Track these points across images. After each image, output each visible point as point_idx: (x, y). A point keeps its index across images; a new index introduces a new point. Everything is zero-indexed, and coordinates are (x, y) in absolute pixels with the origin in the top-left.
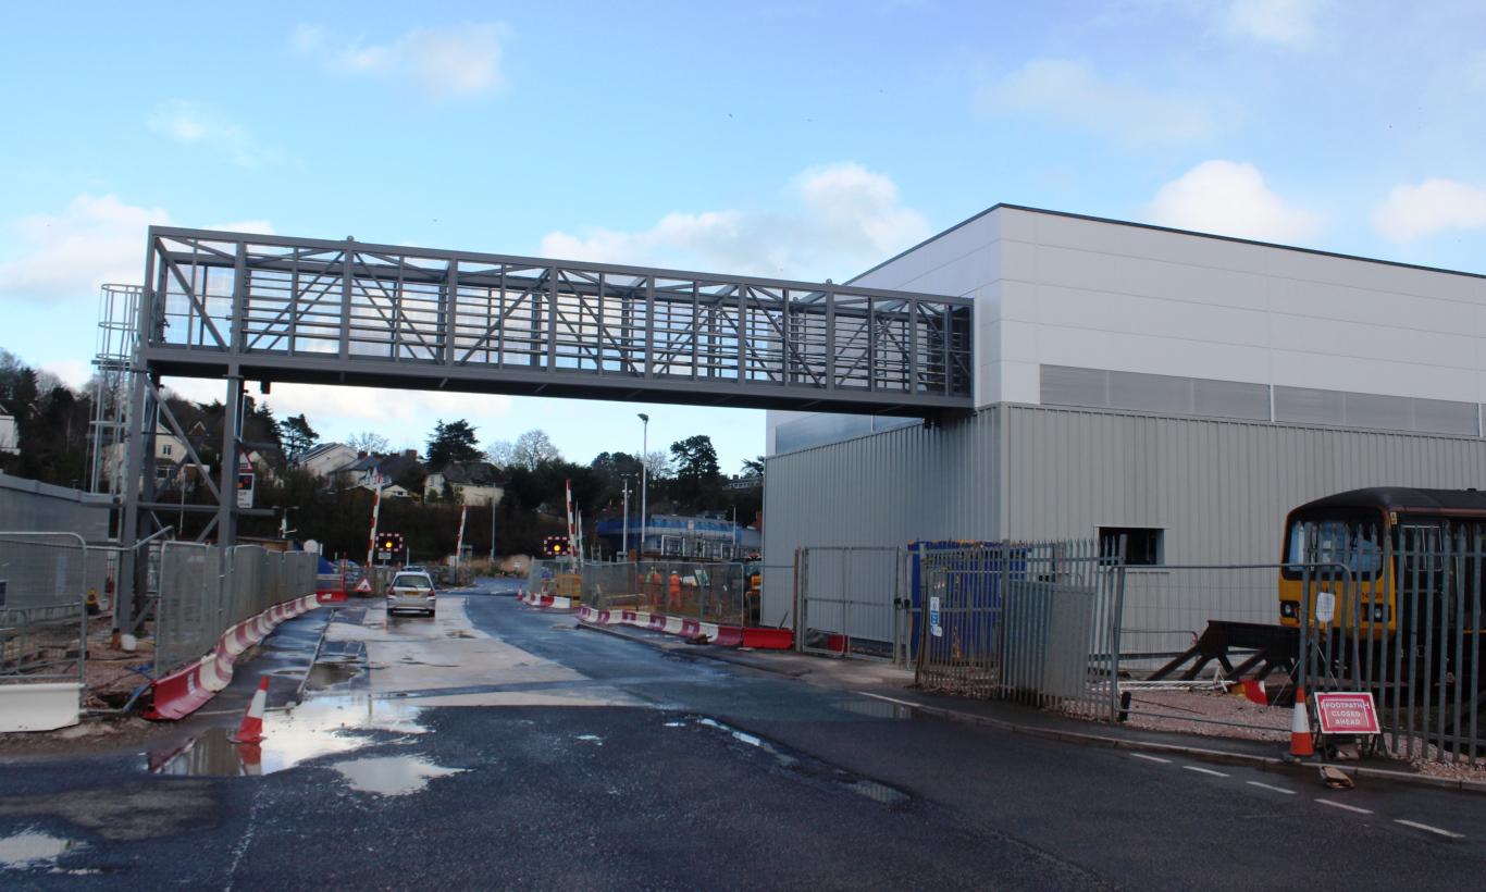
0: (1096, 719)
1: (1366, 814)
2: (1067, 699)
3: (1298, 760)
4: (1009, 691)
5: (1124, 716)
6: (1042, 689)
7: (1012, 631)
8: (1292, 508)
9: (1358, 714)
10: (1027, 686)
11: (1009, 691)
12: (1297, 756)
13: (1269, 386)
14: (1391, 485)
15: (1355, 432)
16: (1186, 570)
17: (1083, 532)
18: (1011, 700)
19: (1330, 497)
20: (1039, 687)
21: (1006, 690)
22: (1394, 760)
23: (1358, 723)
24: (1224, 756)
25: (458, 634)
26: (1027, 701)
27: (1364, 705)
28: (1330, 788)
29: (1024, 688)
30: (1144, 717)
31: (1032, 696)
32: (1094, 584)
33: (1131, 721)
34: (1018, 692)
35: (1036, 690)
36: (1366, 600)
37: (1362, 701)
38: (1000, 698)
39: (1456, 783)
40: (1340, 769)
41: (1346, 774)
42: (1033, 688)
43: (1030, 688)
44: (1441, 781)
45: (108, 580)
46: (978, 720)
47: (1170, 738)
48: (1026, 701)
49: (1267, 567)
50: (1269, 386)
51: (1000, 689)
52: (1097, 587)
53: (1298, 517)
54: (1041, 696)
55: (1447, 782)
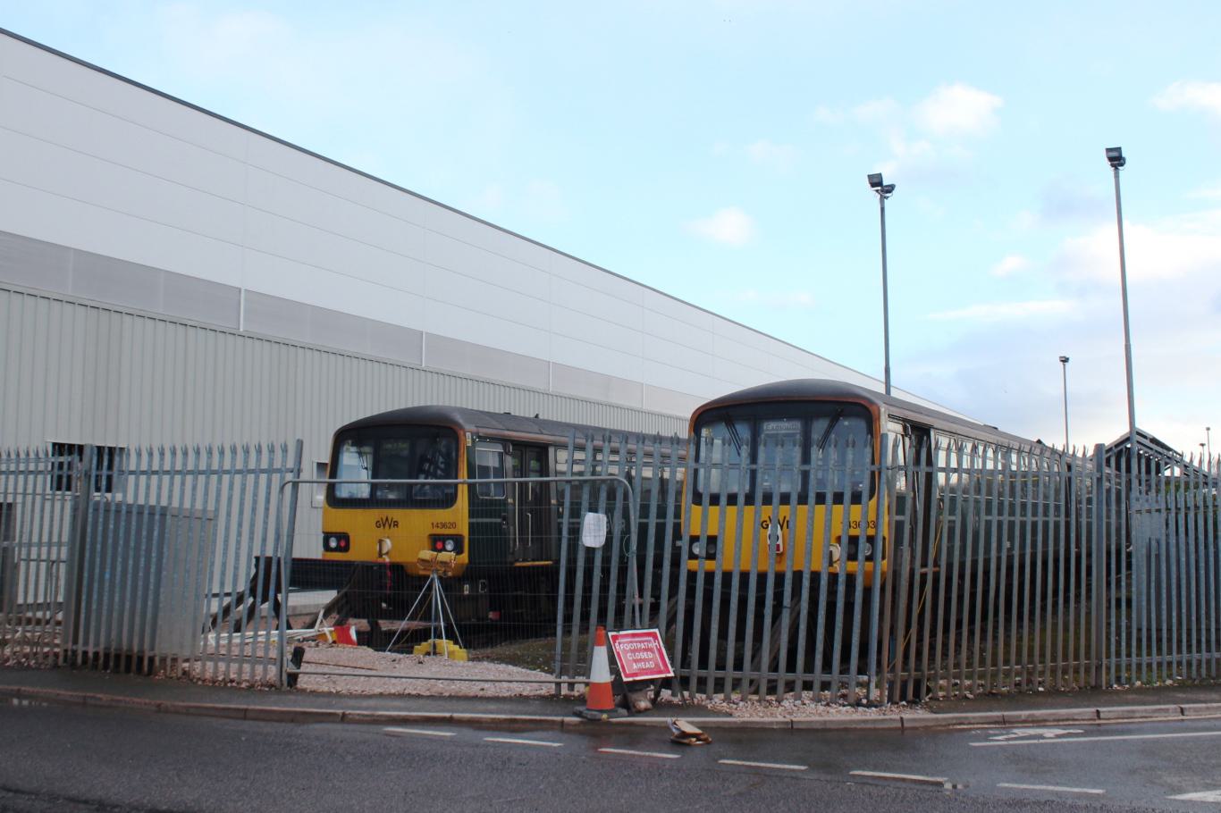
0: (251, 687)
1: (1003, 781)
2: (187, 660)
3: (605, 716)
4: (91, 655)
5: (293, 678)
6: (152, 648)
7: (97, 571)
8: (339, 426)
9: (650, 655)
10: (125, 647)
11: (91, 655)
12: (602, 711)
13: (240, 290)
14: (458, 405)
15: (317, 350)
16: (308, 484)
17: (1035, 440)
18: (95, 667)
19: (383, 414)
20: (146, 646)
21: (85, 653)
22: (678, 705)
23: (651, 665)
24: (506, 720)
25: (1076, 675)
26: (129, 665)
27: (653, 645)
28: (689, 745)
29: (119, 648)
30: (502, 677)
31: (135, 660)
32: (211, 507)
33: (303, 682)
34: (107, 656)
35: (142, 651)
36: (853, 532)
37: (651, 638)
38: (73, 665)
39: (787, 723)
40: (689, 722)
41: (699, 728)
42: (136, 649)
43: (130, 649)
44: (772, 723)
45: (1067, 463)
46: (85, 697)
47: (397, 703)
48: (122, 667)
49: (310, 482)
50: (240, 290)
51: (74, 652)
52: (217, 510)
53: (350, 435)
54: (151, 660)
55: (777, 723)
